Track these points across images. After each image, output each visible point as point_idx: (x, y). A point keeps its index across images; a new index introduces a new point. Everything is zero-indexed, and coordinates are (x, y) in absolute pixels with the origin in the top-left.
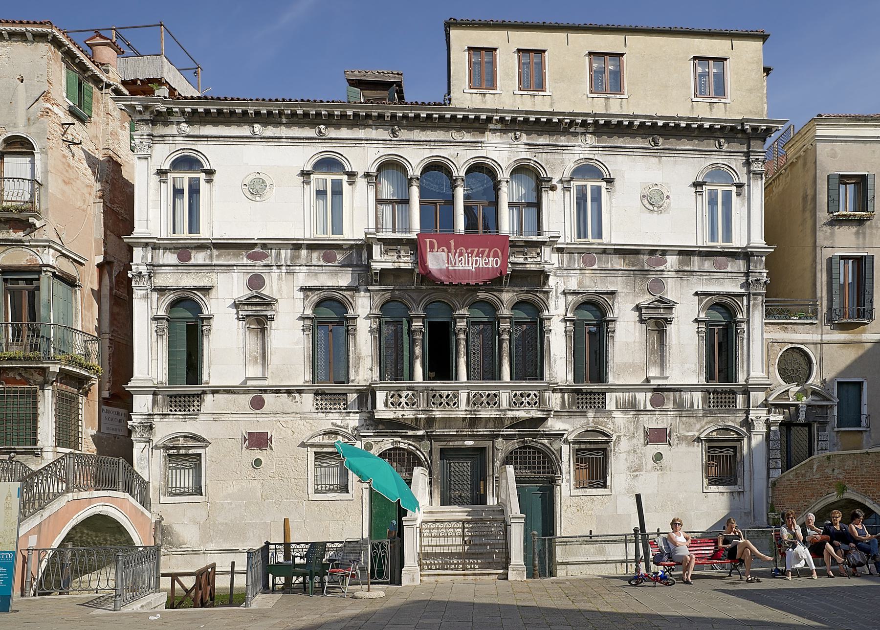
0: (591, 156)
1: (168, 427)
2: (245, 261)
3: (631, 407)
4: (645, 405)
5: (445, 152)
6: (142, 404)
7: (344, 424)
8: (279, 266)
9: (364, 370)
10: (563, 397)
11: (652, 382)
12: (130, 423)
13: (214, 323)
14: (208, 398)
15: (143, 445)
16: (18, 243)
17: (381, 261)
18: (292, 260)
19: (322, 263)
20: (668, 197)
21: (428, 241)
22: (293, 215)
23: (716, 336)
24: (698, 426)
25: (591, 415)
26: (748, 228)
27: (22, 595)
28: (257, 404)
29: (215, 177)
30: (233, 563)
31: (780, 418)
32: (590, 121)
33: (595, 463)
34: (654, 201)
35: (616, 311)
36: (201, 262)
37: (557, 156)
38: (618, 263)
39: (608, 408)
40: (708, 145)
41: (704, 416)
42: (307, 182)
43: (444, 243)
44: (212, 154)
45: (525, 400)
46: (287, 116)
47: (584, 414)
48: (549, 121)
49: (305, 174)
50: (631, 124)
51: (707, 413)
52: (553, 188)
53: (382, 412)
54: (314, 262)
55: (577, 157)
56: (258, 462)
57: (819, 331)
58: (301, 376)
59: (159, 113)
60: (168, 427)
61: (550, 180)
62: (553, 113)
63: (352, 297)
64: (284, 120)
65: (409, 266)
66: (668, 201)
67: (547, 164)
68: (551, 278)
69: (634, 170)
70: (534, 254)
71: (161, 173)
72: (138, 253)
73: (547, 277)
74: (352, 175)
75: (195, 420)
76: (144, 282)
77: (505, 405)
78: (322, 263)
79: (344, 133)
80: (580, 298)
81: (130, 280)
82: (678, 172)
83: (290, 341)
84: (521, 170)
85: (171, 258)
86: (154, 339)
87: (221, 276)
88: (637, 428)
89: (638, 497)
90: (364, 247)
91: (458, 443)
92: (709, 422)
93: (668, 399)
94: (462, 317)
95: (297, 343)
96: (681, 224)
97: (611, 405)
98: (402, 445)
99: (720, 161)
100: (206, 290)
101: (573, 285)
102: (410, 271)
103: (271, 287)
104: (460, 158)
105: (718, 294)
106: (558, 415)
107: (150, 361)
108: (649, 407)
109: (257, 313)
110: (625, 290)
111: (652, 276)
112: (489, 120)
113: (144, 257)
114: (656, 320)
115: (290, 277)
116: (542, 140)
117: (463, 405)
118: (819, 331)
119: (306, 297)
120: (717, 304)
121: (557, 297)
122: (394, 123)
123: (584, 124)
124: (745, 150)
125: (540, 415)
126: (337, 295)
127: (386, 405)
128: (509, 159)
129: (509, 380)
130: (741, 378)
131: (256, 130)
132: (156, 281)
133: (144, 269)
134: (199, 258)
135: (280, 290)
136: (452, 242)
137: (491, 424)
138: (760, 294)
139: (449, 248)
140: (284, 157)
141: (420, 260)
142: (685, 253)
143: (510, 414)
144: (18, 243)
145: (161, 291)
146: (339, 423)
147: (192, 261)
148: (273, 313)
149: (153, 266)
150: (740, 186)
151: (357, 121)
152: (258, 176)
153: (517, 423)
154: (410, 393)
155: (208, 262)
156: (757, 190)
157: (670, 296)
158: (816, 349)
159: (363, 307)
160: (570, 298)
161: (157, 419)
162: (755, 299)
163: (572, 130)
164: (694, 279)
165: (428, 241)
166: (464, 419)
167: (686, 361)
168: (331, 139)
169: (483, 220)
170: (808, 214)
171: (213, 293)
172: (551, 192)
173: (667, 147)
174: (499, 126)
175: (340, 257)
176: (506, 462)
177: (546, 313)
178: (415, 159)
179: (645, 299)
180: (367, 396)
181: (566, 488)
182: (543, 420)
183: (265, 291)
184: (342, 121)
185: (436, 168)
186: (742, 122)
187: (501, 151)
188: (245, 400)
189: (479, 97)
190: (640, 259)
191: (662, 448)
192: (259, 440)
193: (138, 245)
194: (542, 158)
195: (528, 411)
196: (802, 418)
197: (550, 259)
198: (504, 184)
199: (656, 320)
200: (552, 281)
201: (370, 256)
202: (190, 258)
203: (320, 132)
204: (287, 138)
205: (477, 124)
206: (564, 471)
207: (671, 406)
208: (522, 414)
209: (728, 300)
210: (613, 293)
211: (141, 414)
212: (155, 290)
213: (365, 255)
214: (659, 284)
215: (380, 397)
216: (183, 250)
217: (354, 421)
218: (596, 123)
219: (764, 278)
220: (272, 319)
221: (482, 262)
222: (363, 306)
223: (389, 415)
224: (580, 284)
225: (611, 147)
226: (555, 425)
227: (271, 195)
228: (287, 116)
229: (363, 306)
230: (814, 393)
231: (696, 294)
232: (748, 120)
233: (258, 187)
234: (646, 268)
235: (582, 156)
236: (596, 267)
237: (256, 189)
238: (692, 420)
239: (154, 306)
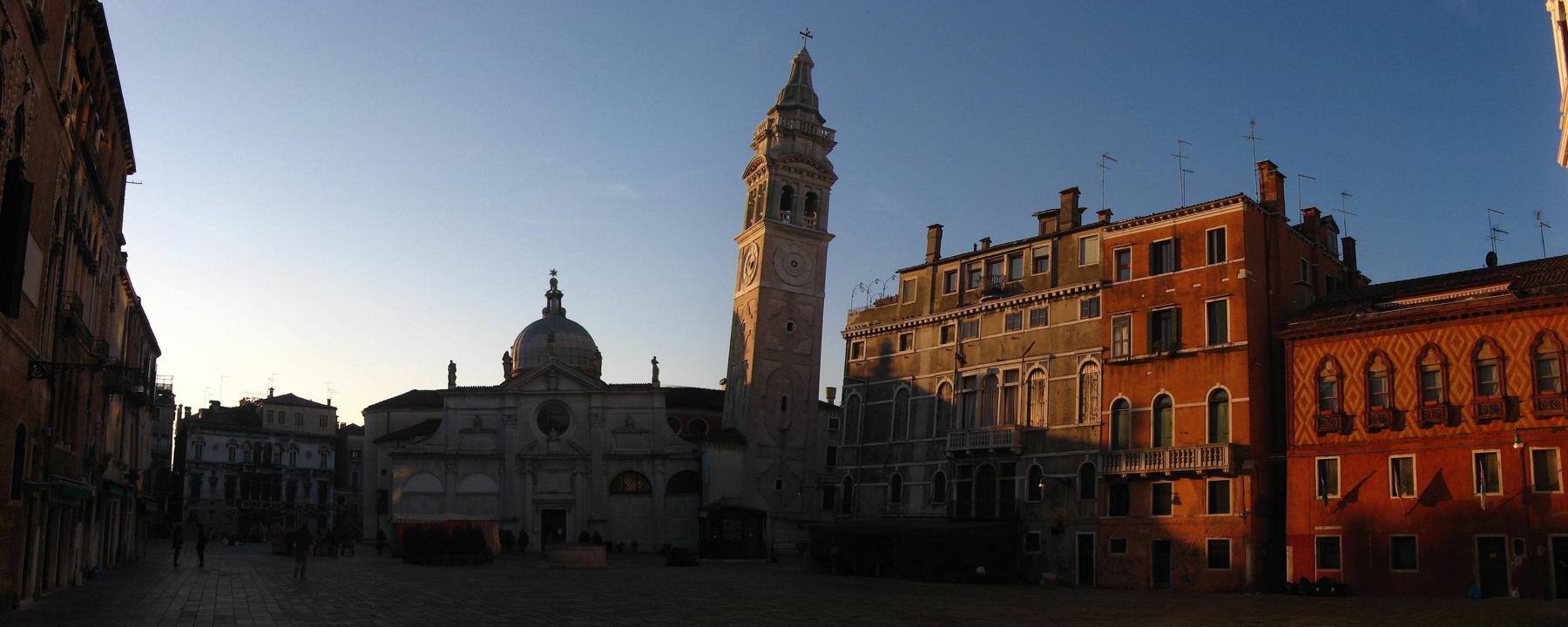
1: (191, 508)
9: (238, 496)
22: (223, 457)
23: (1559, 466)
26: (331, 464)
27: (944, 342)
30: (452, 368)
34: (309, 455)
44: (206, 438)
58: (223, 497)
60: (191, 508)
69: (304, 447)
82: (314, 448)
83: (220, 486)
89: (654, 362)
90: (241, 465)
96: (314, 463)
104: (263, 442)
107: (187, 491)
109: (213, 481)
140: (222, 440)
167: (314, 500)
169: (267, 460)
170: (119, 144)
178: (253, 441)
185: (258, 444)
187: (272, 440)
190: (305, 472)
199: (307, 488)
205: (268, 433)
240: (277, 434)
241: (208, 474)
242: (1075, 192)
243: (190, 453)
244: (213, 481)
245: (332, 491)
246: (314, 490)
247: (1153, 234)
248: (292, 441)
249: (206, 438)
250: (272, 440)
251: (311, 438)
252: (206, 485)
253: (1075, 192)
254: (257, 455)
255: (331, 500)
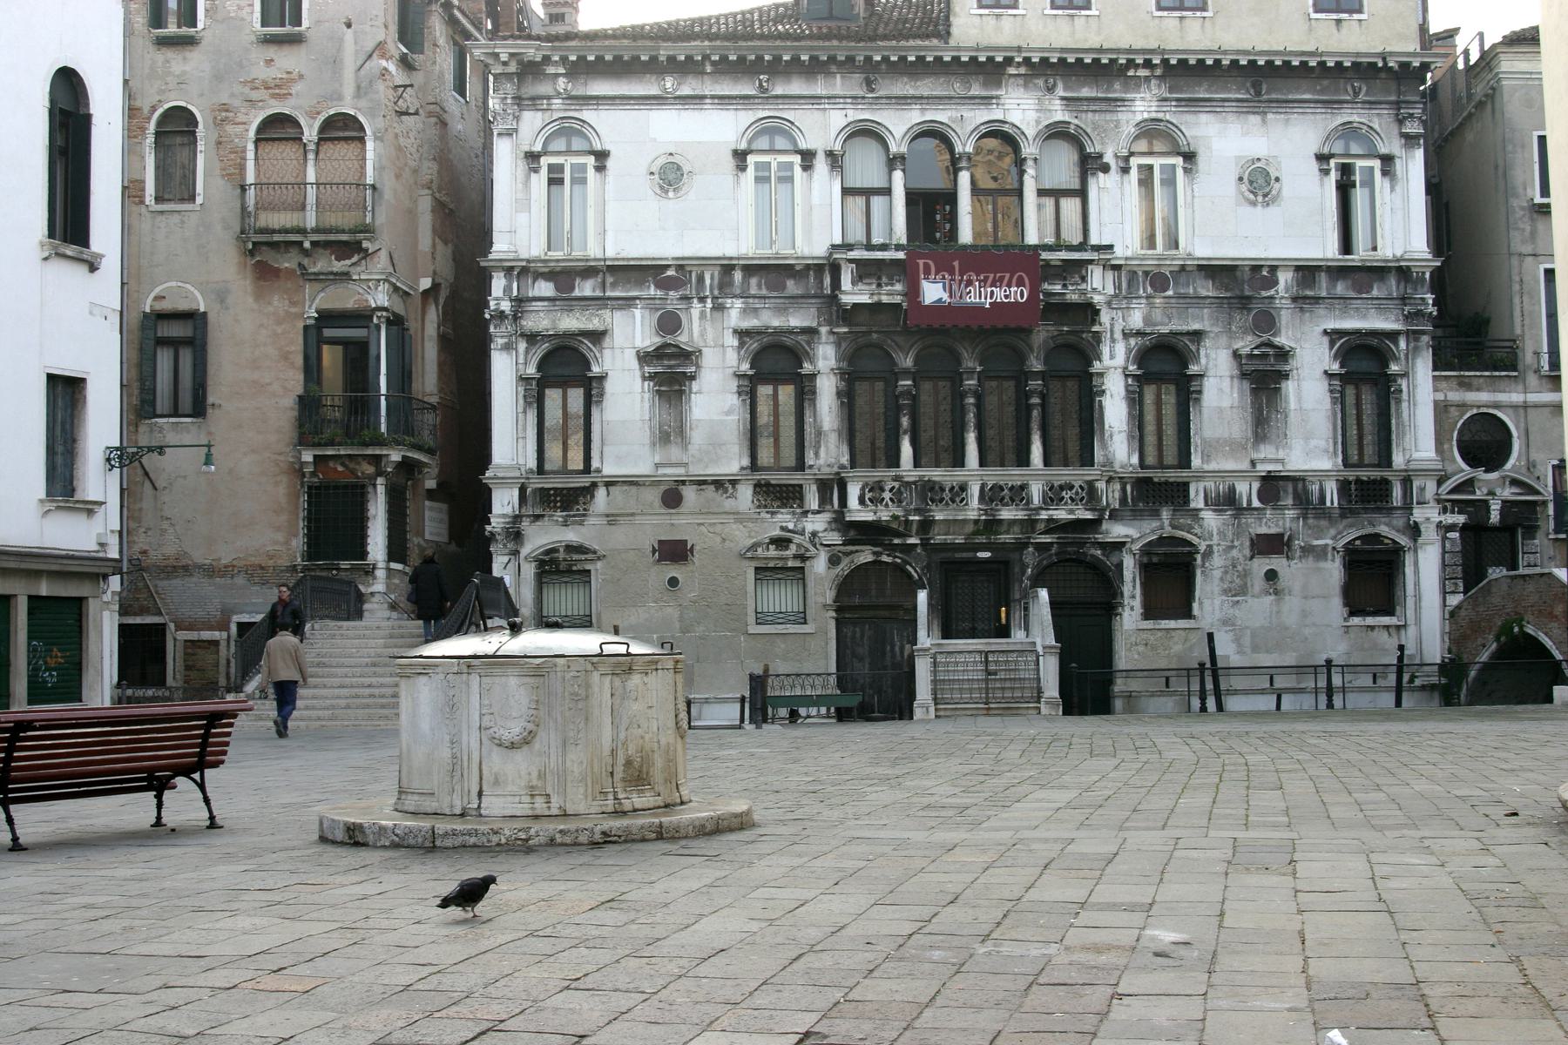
0: (1160, 116)
1: (542, 536)
2: (652, 291)
3: (1227, 501)
4: (1249, 501)
5: (942, 115)
6: (504, 503)
7: (800, 526)
8: (702, 300)
9: (829, 454)
10: (1124, 490)
11: (1259, 467)
12: (488, 528)
13: (609, 386)
14: (601, 493)
15: (506, 559)
16: (345, 276)
17: (854, 293)
18: (721, 287)
19: (764, 292)
20: (1277, 179)
21: (921, 262)
24: (1333, 532)
25: (1166, 514)
26: (1401, 225)
28: (672, 498)
29: (610, 163)
31: (1460, 519)
32: (1156, 61)
33: (1171, 577)
35: (1203, 361)
36: (588, 292)
37: (1108, 116)
38: (1206, 289)
39: (1193, 505)
40: (1337, 91)
41: (1343, 516)
42: (742, 167)
43: (944, 267)
44: (607, 125)
45: (1066, 495)
46: (714, 63)
47: (1155, 514)
48: (1096, 61)
49: (740, 156)
50: (1217, 62)
51: (1344, 512)
52: (1105, 169)
53: (858, 512)
54: (753, 291)
55: (1139, 118)
56: (673, 582)
57: (1520, 387)
58: (732, 462)
59: (532, 64)
60: (542, 536)
61: (1100, 156)
62: (1101, 50)
63: (809, 343)
64: (709, 69)
65: (898, 299)
66: (1277, 185)
67: (1094, 129)
68: (1103, 313)
69: (1227, 138)
70: (1077, 278)
71: (532, 157)
72: (498, 284)
73: (1097, 312)
74: (808, 157)
75: (581, 523)
76: (507, 328)
77: (1036, 500)
78: (764, 292)
79: (796, 87)
80: (1147, 341)
81: (486, 323)
82: (1292, 141)
83: (715, 401)
84: (1057, 133)
85: (545, 288)
86: (520, 409)
87: (618, 315)
88: (1237, 535)
91: (965, 555)
92: (1351, 526)
93: (1286, 491)
94: (971, 372)
95: (728, 413)
96: (1298, 230)
97: (1197, 501)
98: (885, 558)
99: (1355, 118)
100: (597, 336)
101: (1136, 320)
102: (896, 307)
103: (691, 330)
104: (967, 124)
105: (1357, 332)
106: (1114, 515)
108: (1256, 503)
109: (670, 371)
110: (1216, 330)
111: (1256, 306)
112: (1008, 61)
113: (508, 289)
114: (1265, 376)
115: (717, 315)
116: (1086, 92)
117: (975, 502)
118: (1520, 387)
119: (742, 344)
120: (1358, 346)
121: (1113, 340)
122: (871, 71)
123: (1148, 64)
124: (1393, 98)
125: (1089, 515)
126: (787, 341)
127: (862, 501)
128: (1038, 122)
129: (1041, 466)
130: (1398, 460)
131: (668, 85)
132: (524, 323)
133: (506, 306)
134: (586, 288)
135: (703, 334)
136: (956, 264)
137: (1016, 529)
138: (1423, 332)
139: (952, 273)
141: (913, 292)
142: (1307, 272)
143: (1044, 515)
144: (345, 276)
145: (532, 338)
146: (791, 526)
147: (577, 293)
148: (693, 369)
149: (520, 302)
150: (1387, 160)
151: (815, 68)
152: (671, 159)
153: (1054, 526)
154: (896, 485)
155: (598, 293)
156: (1414, 167)
157: (1282, 340)
158: (1517, 416)
159: (825, 358)
160: (1133, 341)
161: (525, 523)
162: (1417, 340)
163: (1131, 73)
164: (1321, 310)
165: (921, 262)
166: (976, 522)
167: (1310, 443)
168: (777, 97)
171: (607, 342)
172: (1101, 175)
173: (1274, 96)
174: (1022, 70)
175: (792, 287)
176: (1037, 582)
177: (1097, 364)
178: (898, 124)
179: (1246, 344)
180: (832, 487)
181: (1130, 618)
182: (1094, 524)
183: (682, 339)
184: (795, 68)
186: (1384, 56)
187: (1023, 109)
188: (653, 496)
189: (992, 21)
190: (1239, 286)
191: (1277, 563)
192: (674, 552)
193: (497, 268)
194: (1085, 121)
195: (1071, 512)
196: (1495, 517)
197: (1099, 284)
198: (1030, 163)
199: (1265, 376)
200: (1105, 317)
201: (836, 284)
202: (572, 289)
203: (761, 85)
204: (713, 97)
205: (989, 70)
206: (1126, 594)
207: (1290, 501)
208: (1061, 514)
209: (1375, 342)
210: (1197, 335)
211: (504, 516)
212: (522, 335)
213: (827, 280)
214: (1266, 322)
215: (854, 492)
216: (564, 276)
217: (817, 523)
218: (1165, 62)
219: (1431, 309)
220: (693, 378)
221: (1000, 294)
222: (825, 359)
223: (867, 516)
224: (1147, 320)
225: (1190, 100)
226: (1117, 531)
227: (694, 189)
228: (714, 63)
229: (825, 359)
230: (1515, 482)
231: (1325, 332)
232: (1391, 54)
233: (671, 177)
234: (1247, 293)
235: (1146, 115)
236: (1170, 293)
237: (670, 177)
238: (1324, 523)
239: (521, 360)
240: (1048, 69)
241: (629, 334)
242: (93, 268)
243: (518, 227)
244: (670, 371)
245: (1422, 390)
246: (1309, 390)
247: (131, 191)
248: (1144, 105)
249: (607, 125)
250: (1023, 109)
251: (1263, 81)
252: (626, 396)
253: (93, 268)
254: (931, 210)
255: (1419, 441)
